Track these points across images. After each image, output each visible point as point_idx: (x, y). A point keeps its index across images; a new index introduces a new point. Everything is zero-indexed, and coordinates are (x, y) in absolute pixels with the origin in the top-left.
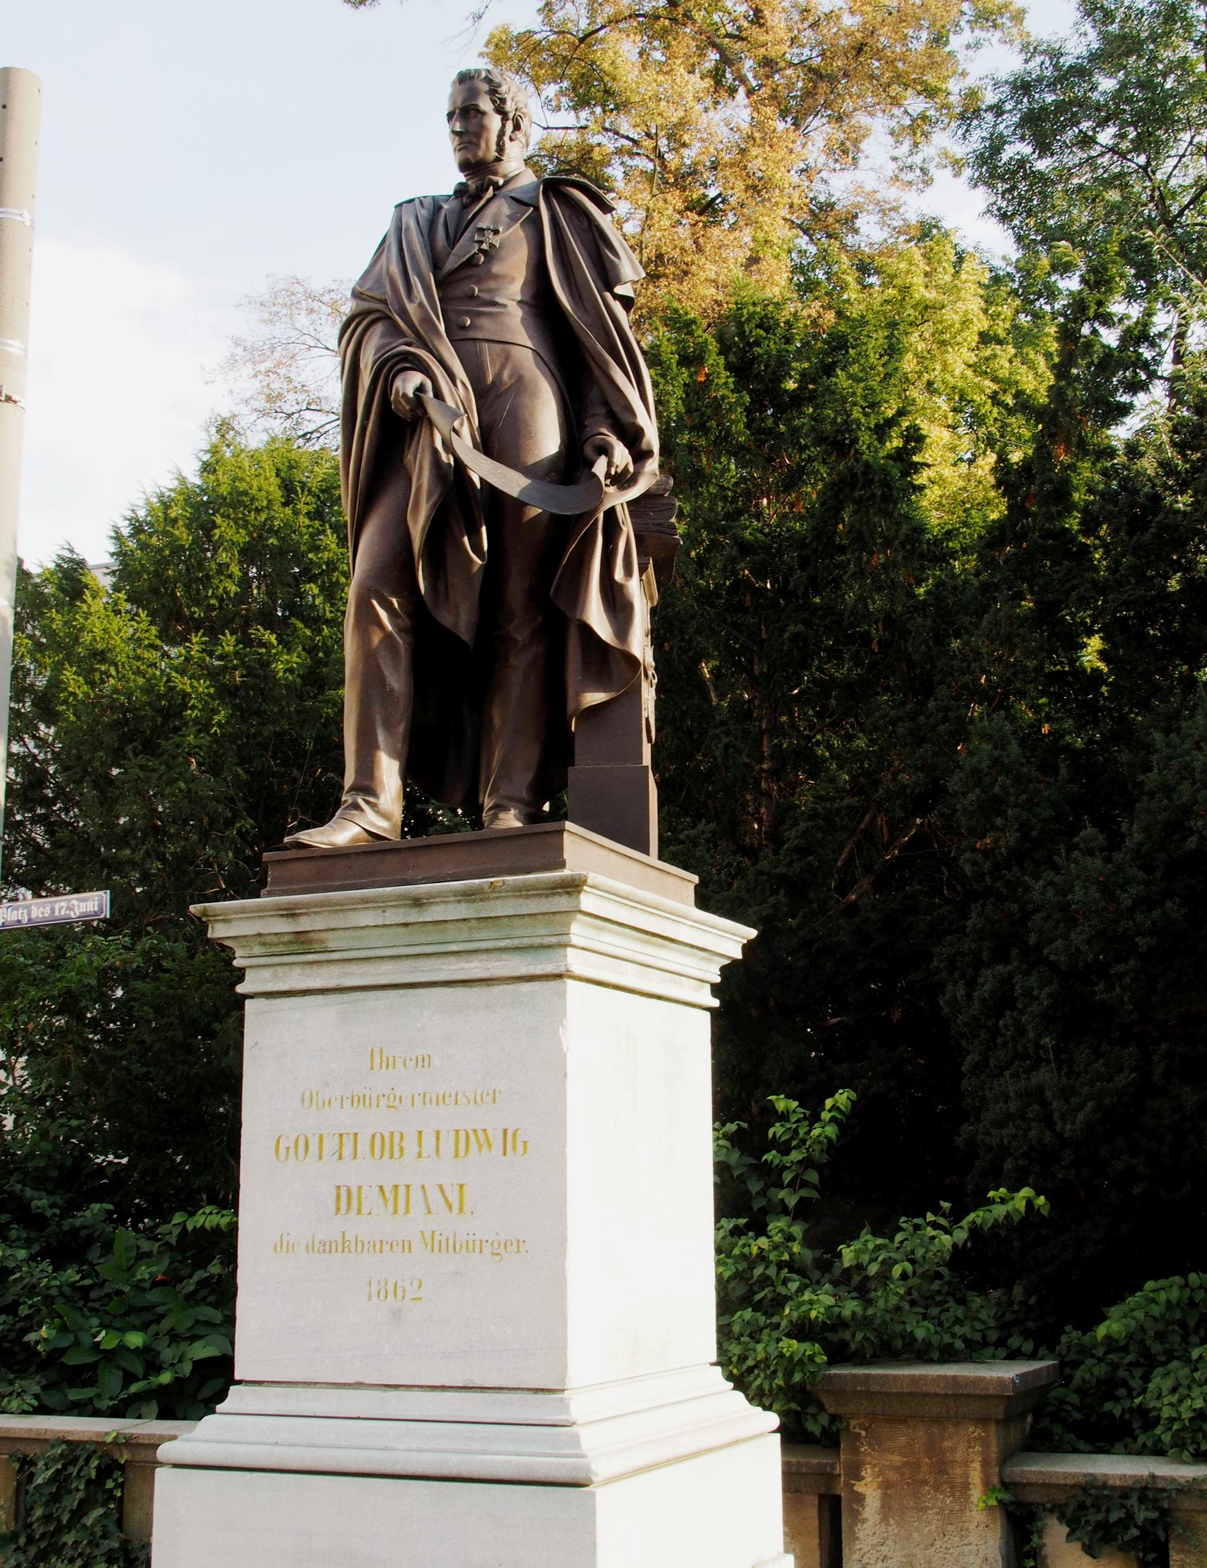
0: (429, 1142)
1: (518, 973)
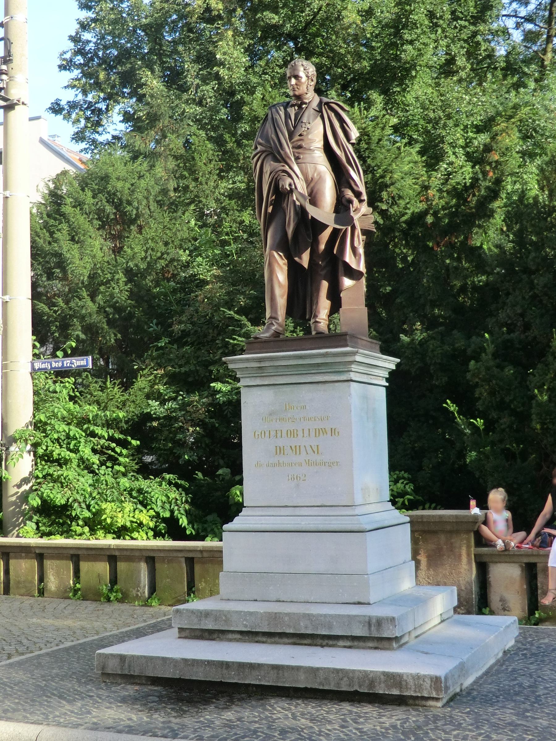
0: (306, 432)
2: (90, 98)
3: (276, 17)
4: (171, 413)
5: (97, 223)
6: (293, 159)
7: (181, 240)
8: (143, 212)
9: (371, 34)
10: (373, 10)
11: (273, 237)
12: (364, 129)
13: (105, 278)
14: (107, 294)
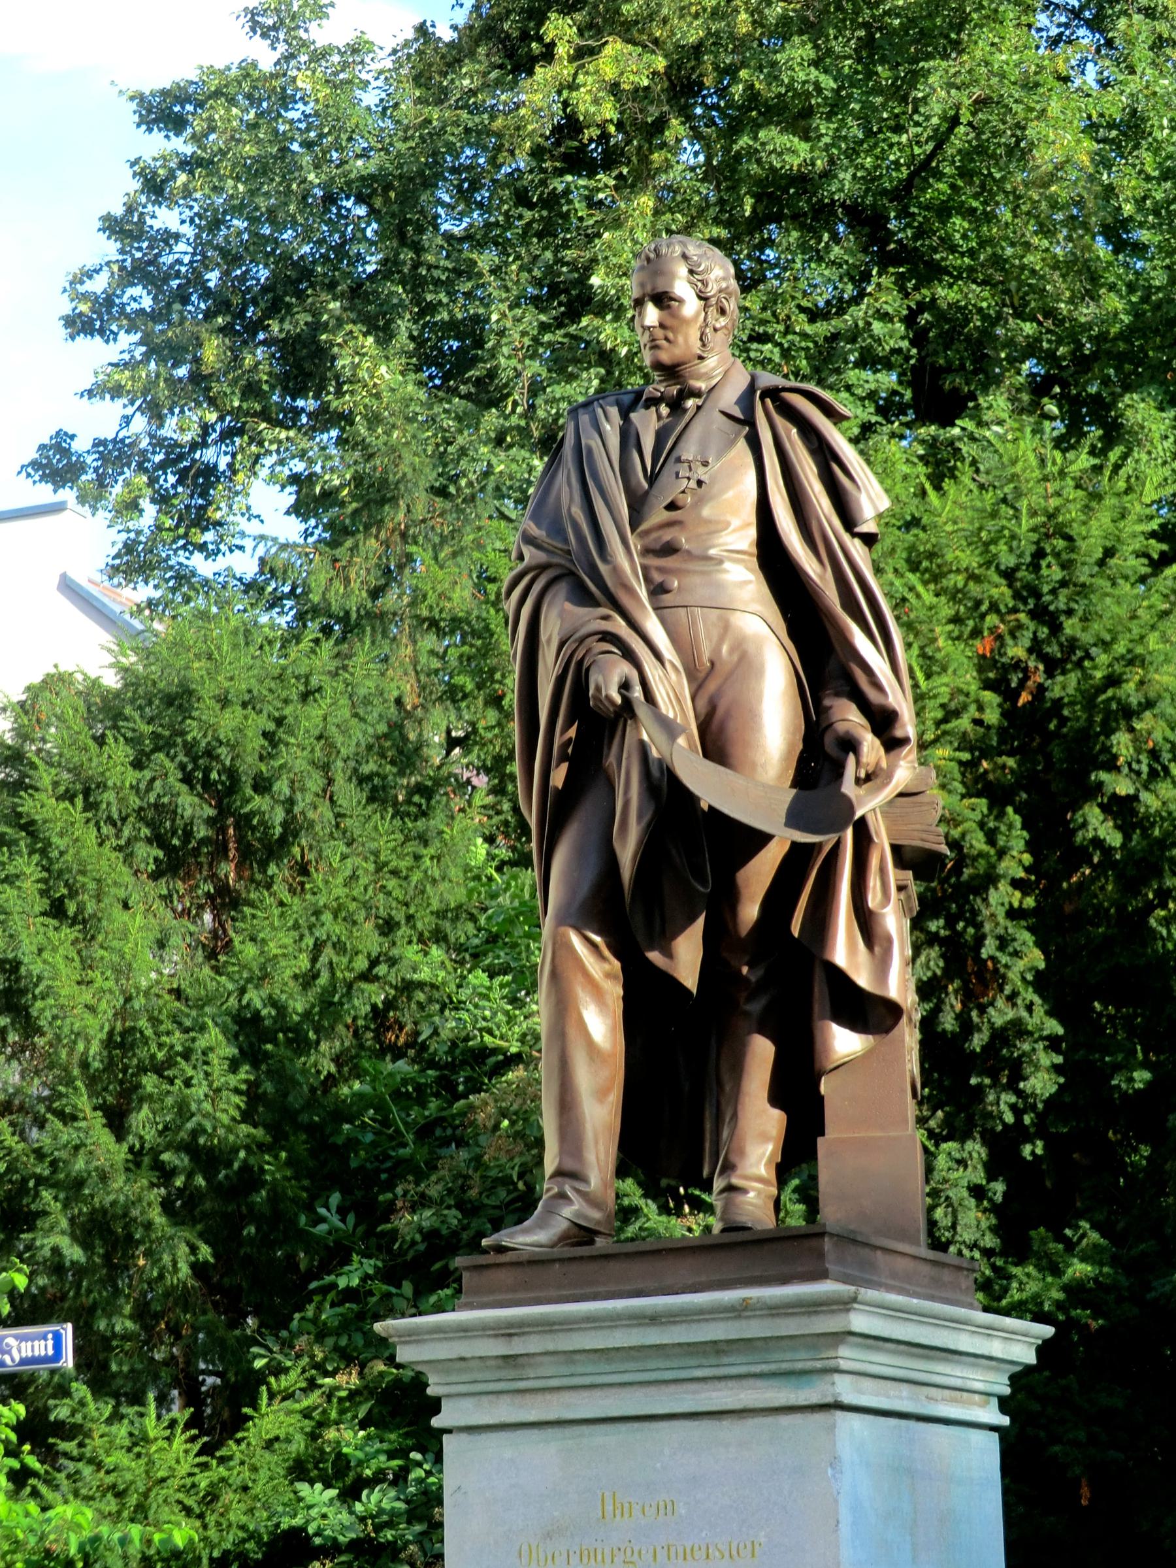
1: (776, 1404)
2: (169, 429)
3: (803, 147)
4: (378, 1528)
5: (148, 854)
6: (643, 593)
7: (440, 914)
8: (311, 815)
9: (1140, 202)
10: (1145, 120)
11: (566, 874)
12: (1051, 516)
13: (160, 1046)
14: (169, 1101)
